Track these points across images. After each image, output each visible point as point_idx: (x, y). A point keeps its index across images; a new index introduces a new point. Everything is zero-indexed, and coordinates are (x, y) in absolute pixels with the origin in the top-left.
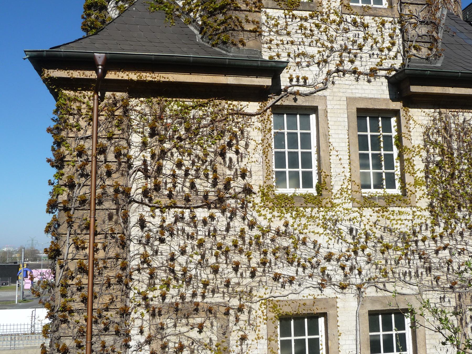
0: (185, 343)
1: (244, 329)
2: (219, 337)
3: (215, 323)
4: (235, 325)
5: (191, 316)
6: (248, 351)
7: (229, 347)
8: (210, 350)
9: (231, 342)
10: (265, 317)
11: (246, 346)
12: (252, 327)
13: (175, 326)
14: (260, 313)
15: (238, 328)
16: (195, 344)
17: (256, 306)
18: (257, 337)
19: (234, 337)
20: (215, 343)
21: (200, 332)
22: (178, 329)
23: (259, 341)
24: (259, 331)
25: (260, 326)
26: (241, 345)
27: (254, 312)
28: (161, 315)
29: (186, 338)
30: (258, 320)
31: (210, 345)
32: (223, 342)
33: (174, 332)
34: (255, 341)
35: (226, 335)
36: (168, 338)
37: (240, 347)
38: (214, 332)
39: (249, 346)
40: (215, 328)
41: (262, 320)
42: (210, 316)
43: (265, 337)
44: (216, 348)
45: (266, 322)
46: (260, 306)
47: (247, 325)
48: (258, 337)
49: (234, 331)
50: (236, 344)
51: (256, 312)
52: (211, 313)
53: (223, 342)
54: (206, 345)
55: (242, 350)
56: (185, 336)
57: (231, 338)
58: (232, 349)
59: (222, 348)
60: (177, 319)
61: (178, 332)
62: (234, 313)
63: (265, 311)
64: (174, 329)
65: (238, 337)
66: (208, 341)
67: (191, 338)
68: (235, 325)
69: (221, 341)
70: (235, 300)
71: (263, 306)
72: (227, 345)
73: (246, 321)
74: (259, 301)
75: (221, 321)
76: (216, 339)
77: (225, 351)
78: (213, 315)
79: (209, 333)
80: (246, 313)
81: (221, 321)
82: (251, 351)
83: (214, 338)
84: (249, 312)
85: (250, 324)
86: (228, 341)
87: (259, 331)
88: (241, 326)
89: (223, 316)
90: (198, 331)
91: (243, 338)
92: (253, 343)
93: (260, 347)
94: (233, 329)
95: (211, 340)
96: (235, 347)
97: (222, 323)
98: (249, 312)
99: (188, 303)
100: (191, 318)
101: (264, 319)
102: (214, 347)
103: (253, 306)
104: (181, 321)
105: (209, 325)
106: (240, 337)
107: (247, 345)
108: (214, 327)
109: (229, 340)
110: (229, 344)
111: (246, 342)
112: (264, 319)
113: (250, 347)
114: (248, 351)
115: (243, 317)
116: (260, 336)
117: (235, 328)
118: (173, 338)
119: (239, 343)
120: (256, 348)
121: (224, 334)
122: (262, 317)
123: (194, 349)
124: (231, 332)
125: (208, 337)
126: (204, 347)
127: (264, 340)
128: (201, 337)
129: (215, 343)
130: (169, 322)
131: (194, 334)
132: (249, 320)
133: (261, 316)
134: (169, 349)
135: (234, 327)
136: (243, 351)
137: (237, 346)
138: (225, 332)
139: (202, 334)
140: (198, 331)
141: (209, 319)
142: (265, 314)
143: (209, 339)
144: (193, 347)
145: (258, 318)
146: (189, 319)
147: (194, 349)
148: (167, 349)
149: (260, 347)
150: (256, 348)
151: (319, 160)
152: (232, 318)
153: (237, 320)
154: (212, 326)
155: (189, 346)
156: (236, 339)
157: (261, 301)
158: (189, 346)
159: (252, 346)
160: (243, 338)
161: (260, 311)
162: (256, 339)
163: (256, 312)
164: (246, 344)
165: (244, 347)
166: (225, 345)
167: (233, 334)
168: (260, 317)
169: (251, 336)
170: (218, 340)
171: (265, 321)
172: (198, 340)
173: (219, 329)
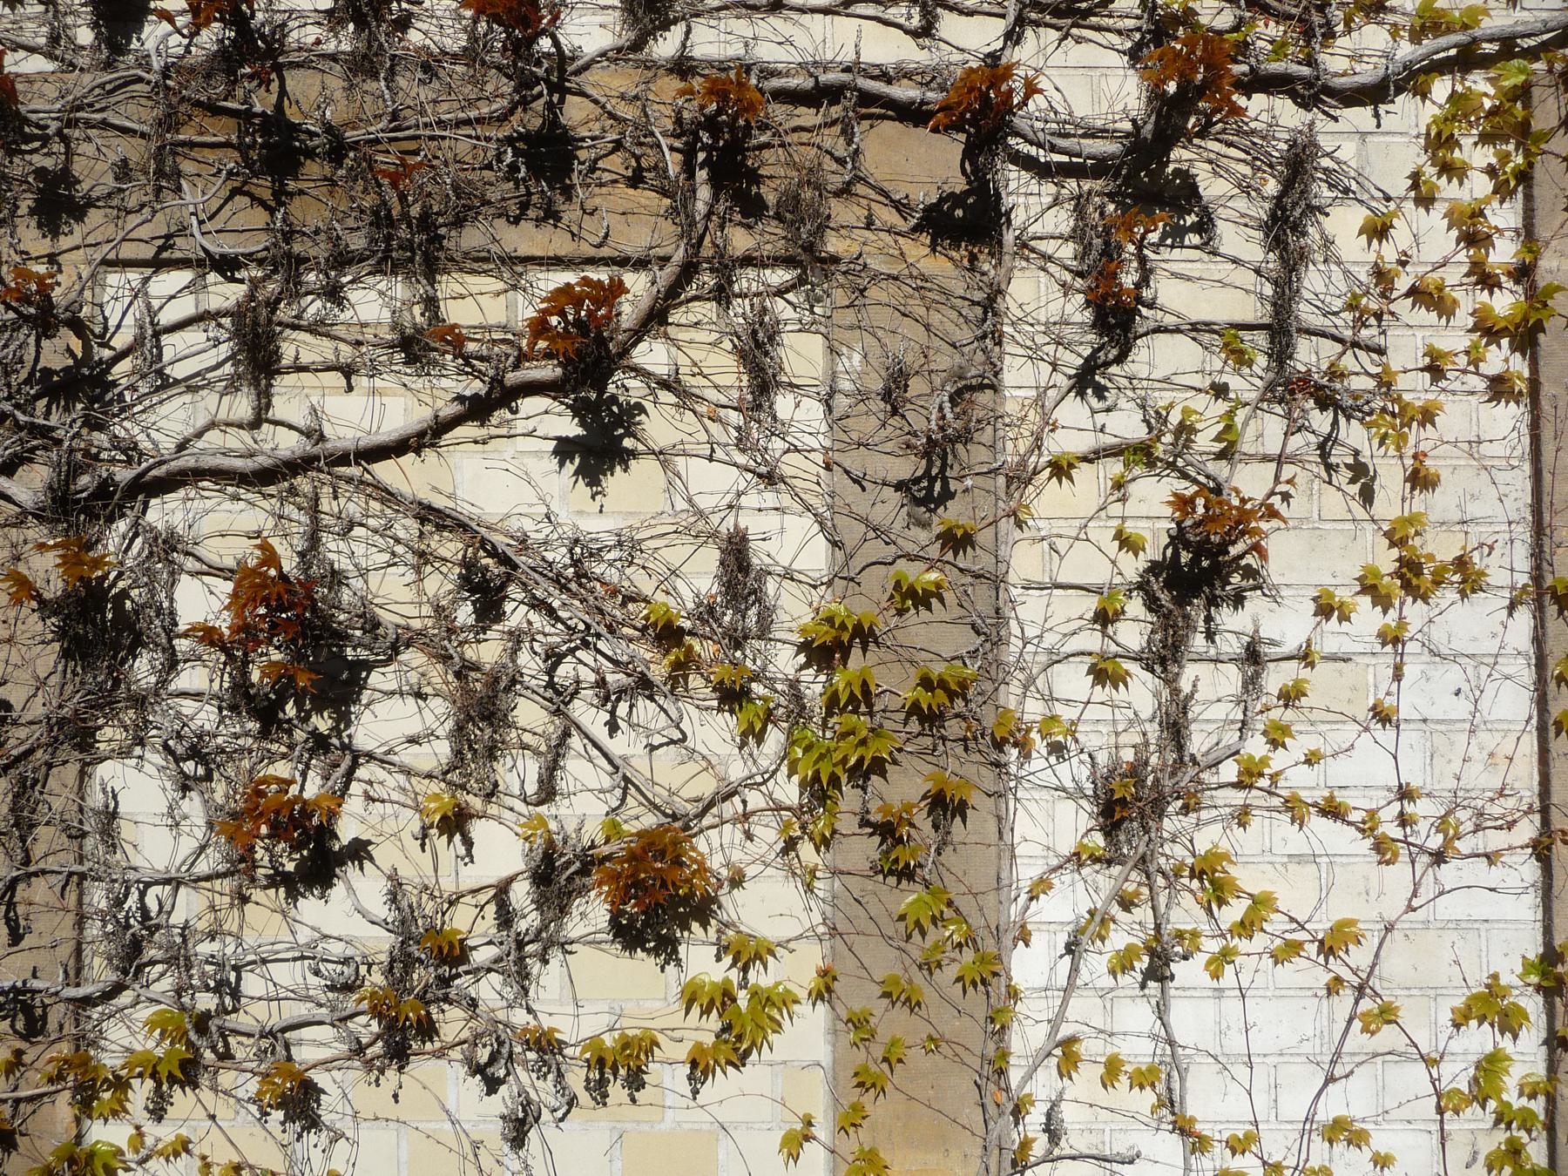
0: (391, 585)
1: (1205, 441)
2: (852, 532)
3: (801, 354)
4: (1086, 381)
5: (472, 238)
6: (1256, 746)
7: (995, 673)
8: (732, 696)
9: (1030, 611)
10: (1504, 302)
11: (1231, 678)
12: (1321, 421)
13: (258, 359)
14: (1428, 239)
15: (1127, 425)
16: (516, 614)
17: (1379, 147)
18: (1387, 560)
19: (1073, 546)
20: (795, 610)
21: (599, 450)
22: (292, 399)
23: (1415, 612)
24: (1420, 480)
25: (1427, 416)
26: (1165, 656)
27: (1343, 224)
28: (78, 212)
29: (406, 527)
30: (1410, 337)
31: (737, 641)
32: (915, 598)
33: (237, 440)
34: (1368, 618)
35: (954, 513)
36: (164, 512)
37: (1142, 691)
38: (791, 465)
39: (1276, 678)
40: (799, 413)
41: (1455, 338)
42: (740, 241)
43: (1509, 566)
44: (814, 686)
45: (1519, 365)
46: (1439, 142)
47: (1244, 386)
48: (1409, 570)
49: (1061, 469)
50: (1092, 640)
51: (1378, 230)
52: (752, 209)
53: (915, 598)
54: (667, 635)
55: (1175, 728)
56: (387, 496)
57: (1025, 561)
58: (1034, 709)
59: (897, 687)
60: (288, 265)
61: (288, 444)
62: (1062, 220)
63: (1504, 216)
64: (242, 405)
65: (1126, 542)
66: (701, 575)
67: (460, 526)
68: (1086, 381)
69: (877, 584)
70: (1075, 53)
71: (1476, 155)
72: (965, 640)
73: (1228, 339)
74: (1413, 80)
75: (880, 317)
76: (816, 558)
77: (930, 719)
78: (770, 237)
79: (712, 482)
80: (1240, 239)
81: (880, 317)
82: (1297, 747)
83: (791, 543)
84: (1285, 227)
85: (1287, 389)
86: (982, 592)
87: (1420, 480)
88: (1177, 404)
89: (917, 250)
90: (564, 449)
91: (1200, 569)
92: (1333, 636)
93: (1426, 692)
94: (1062, 443)
95: (736, 552)
96: (1073, 681)
97: (906, 341)
98: (1285, 227)
99: (429, 65)
100: (479, 262)
101: (1487, 329)
102: (785, 661)
103: (1343, 135)
104: (334, 294)
105: (724, 373)
106: (1155, 549)
107: (1253, 656)
108: (783, 404)
109: (997, 582)
110: (990, 632)
111: (1227, 618)
112: (1487, 329)
113: (1290, 697)
114: (1256, 746)
115: (1202, 285)
116: (1440, 547)
117: (1075, 425)
118: (226, 526)
119: (1134, 631)
120: (1382, 716)
121: (925, 494)
122: (1468, 301)
123: (504, 683)
124: (1020, 478)
125: (696, 526)
126: (644, 652)
127: (1489, 605)
128: (597, 526)
129: (795, 610)
130: (184, 307)
131: (511, 478)
132: (1281, 330)
133: (1454, 275)
134: (172, 664)
135: (1073, 411)
136: (1198, 742)
137: (1104, 673)
138: (940, 464)
139: (616, 481)
140: (564, 449)
141: (722, 295)
142: (1504, 253)
143: (710, 558)
144: (489, 651)
145: (1403, 306)
146: (448, 285)
147: (504, 683)
148: (143, 669)
149: (1426, 692)
150: (1382, 716)
151: (1443, 50)
152: (1041, 296)
153: (1117, 319)
154: (764, 380)
155: (439, 641)
156: (1100, 574)
157: (1441, 88)
158: (439, 641)
159: (1320, 679)
160: (1200, 569)
161: (1435, 219)
162: (1369, 587)
163: (1378, 230)
164: (1231, 645)
165: (1211, 684)
166: (938, 638)
167: (1051, 502)
168: (1427, 296)
169: (1313, 549)
170: (843, 578)
171: (1498, 358)
172: (559, 556)
173: (865, 425)
